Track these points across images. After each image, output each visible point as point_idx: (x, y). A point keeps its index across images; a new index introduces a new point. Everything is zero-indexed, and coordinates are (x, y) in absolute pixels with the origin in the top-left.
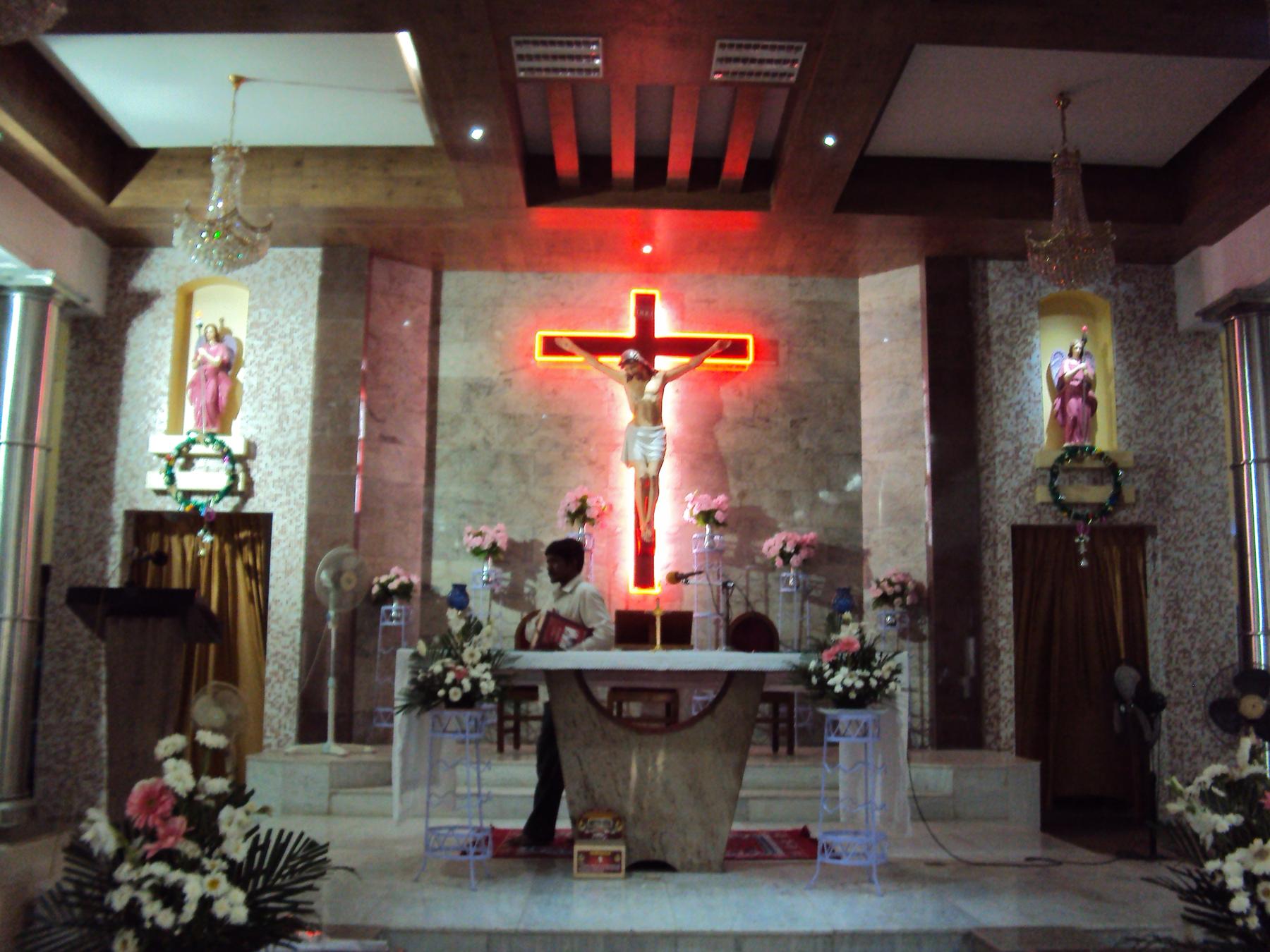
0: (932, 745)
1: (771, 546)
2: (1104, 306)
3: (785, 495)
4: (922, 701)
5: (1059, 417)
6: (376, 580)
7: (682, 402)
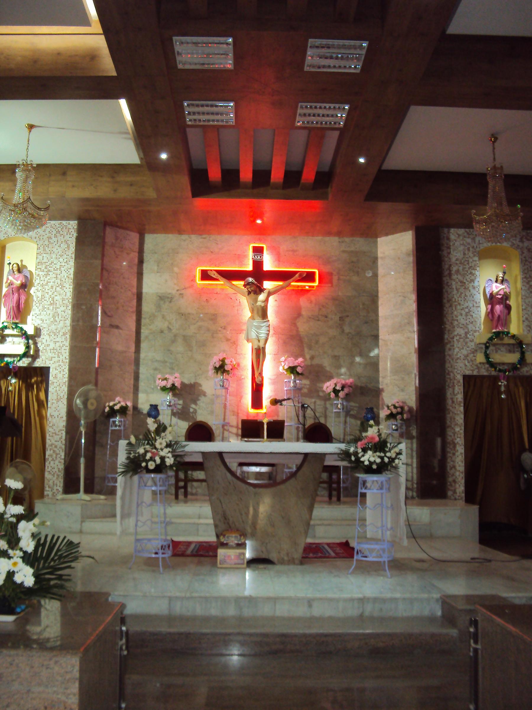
0: (418, 496)
1: (328, 386)
2: (515, 254)
3: (336, 358)
4: (412, 473)
5: (490, 316)
6: (107, 404)
7: (279, 307)
